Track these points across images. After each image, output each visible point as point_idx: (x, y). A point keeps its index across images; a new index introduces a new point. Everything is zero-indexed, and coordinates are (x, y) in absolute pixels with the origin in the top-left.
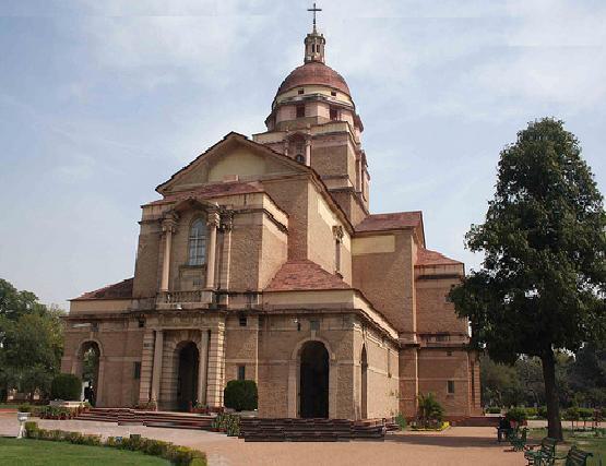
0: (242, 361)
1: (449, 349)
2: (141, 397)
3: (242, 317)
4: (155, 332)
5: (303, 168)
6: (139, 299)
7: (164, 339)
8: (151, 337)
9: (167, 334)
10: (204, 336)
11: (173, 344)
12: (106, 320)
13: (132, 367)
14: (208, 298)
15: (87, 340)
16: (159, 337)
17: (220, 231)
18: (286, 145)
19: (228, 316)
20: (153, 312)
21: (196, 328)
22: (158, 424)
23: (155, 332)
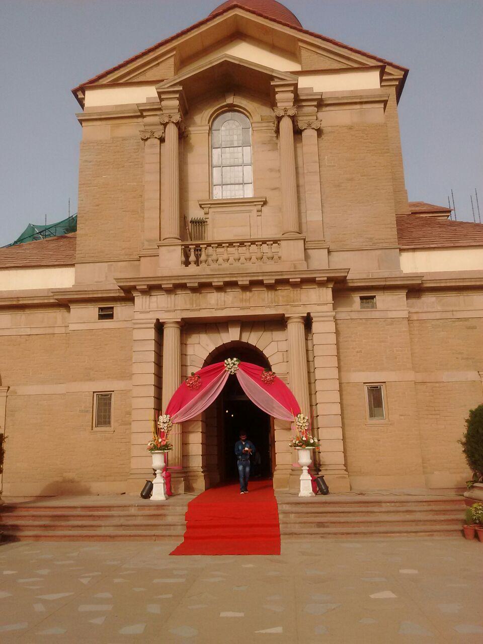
0: (375, 377)
8: (151, 334)
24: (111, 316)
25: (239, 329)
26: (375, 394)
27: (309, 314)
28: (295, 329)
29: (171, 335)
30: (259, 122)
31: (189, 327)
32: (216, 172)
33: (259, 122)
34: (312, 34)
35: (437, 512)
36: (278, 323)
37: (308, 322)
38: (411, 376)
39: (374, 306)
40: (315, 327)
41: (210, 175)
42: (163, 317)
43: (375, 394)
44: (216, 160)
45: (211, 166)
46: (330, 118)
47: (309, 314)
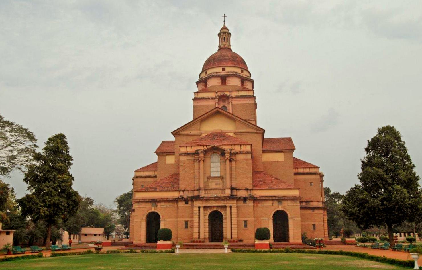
0: (245, 219)
1: (313, 209)
2: (194, 236)
3: (245, 199)
4: (199, 208)
5: (403, 232)
6: (183, 191)
7: (204, 210)
8: (198, 209)
9: (205, 208)
10: (228, 209)
11: (209, 212)
12: (163, 201)
13: (184, 223)
14: (228, 192)
15: (151, 211)
16: (202, 210)
17: (230, 161)
18: (217, 100)
19: (238, 199)
20: (198, 198)
21: (223, 205)
22: (209, 113)
23: (199, 208)
24: (188, 204)
25: (253, 201)
26: (245, 222)
27: (231, 206)
28: (228, 209)
29: (202, 210)
30: (418, 240)
31: (205, 208)
32: (212, 169)
33: (418, 240)
34: (212, 110)
35: (253, 245)
36: (225, 207)
37: (231, 207)
38: (253, 219)
39: (246, 203)
40: (232, 209)
41: (210, 169)
42: (200, 205)
43: (245, 222)
44: (212, 166)
45: (210, 167)
46: (240, 157)
47: (231, 206)
